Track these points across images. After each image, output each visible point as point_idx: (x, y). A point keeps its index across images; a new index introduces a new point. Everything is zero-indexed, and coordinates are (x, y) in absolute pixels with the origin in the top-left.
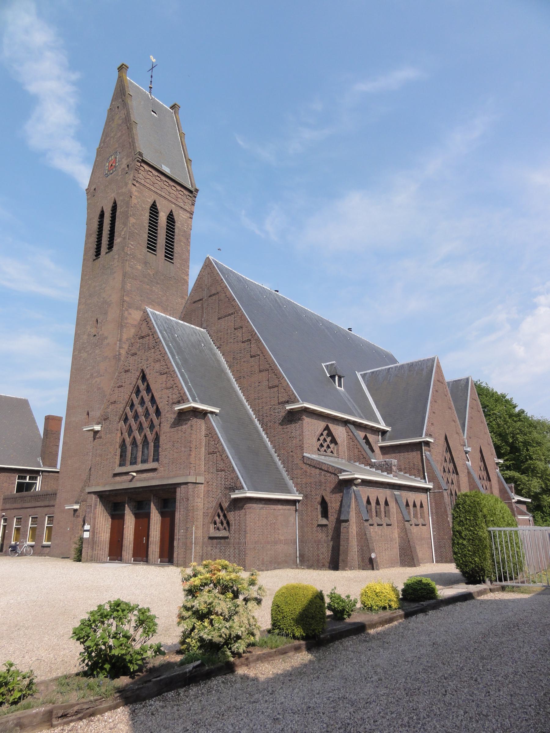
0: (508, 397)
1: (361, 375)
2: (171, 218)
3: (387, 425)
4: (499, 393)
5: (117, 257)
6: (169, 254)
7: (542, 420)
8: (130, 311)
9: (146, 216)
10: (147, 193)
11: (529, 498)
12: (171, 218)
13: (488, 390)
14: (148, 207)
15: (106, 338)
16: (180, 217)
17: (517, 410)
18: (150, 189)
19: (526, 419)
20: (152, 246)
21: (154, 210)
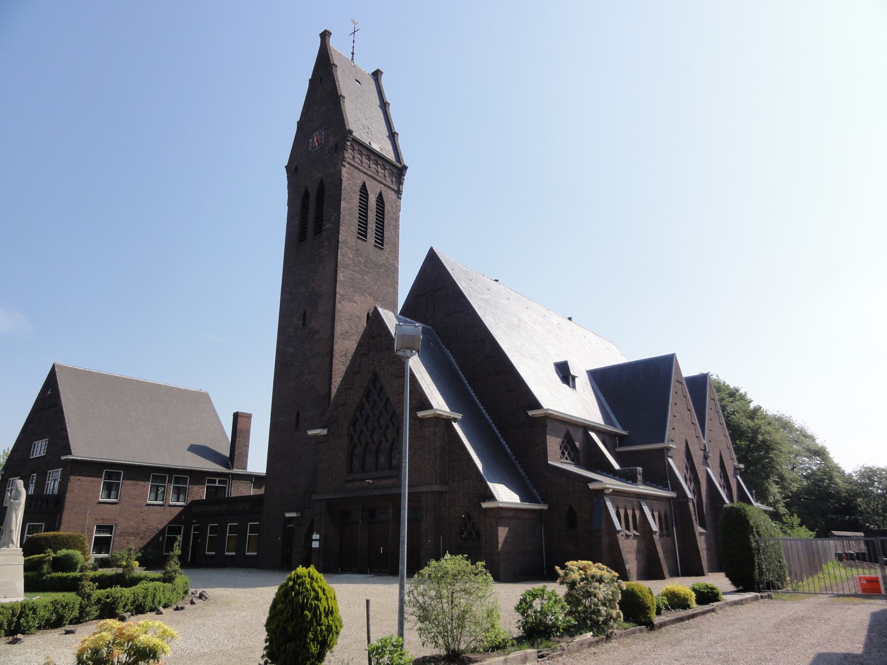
0: (742, 391)
1: (429, 406)
2: (380, 199)
3: (624, 429)
4: (731, 387)
5: (326, 244)
6: (380, 241)
7: (778, 415)
8: (344, 303)
9: (357, 197)
10: (356, 173)
11: (323, 427)
12: (380, 199)
13: (719, 383)
14: (358, 189)
15: (318, 332)
16: (389, 196)
17: (752, 406)
18: (359, 170)
19: (765, 417)
20: (363, 234)
21: (364, 190)
